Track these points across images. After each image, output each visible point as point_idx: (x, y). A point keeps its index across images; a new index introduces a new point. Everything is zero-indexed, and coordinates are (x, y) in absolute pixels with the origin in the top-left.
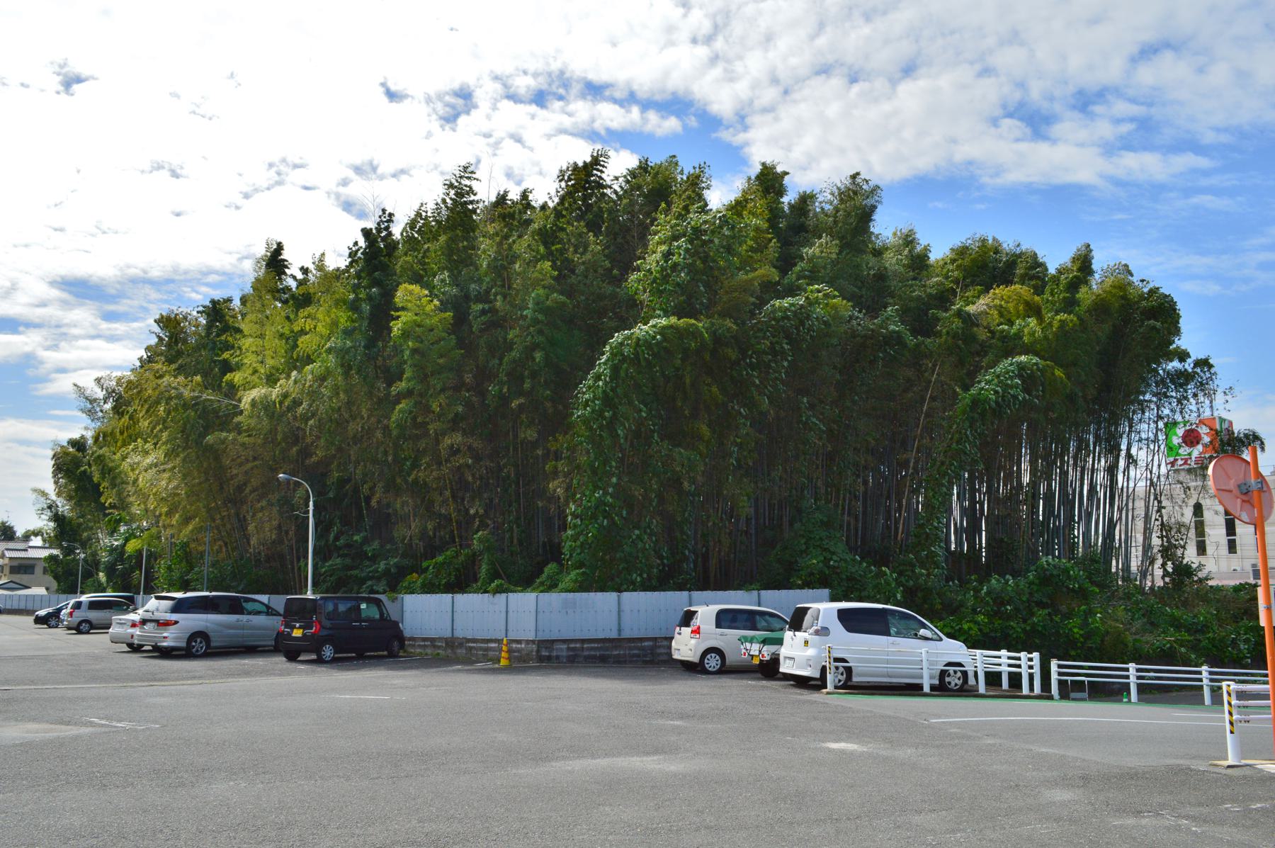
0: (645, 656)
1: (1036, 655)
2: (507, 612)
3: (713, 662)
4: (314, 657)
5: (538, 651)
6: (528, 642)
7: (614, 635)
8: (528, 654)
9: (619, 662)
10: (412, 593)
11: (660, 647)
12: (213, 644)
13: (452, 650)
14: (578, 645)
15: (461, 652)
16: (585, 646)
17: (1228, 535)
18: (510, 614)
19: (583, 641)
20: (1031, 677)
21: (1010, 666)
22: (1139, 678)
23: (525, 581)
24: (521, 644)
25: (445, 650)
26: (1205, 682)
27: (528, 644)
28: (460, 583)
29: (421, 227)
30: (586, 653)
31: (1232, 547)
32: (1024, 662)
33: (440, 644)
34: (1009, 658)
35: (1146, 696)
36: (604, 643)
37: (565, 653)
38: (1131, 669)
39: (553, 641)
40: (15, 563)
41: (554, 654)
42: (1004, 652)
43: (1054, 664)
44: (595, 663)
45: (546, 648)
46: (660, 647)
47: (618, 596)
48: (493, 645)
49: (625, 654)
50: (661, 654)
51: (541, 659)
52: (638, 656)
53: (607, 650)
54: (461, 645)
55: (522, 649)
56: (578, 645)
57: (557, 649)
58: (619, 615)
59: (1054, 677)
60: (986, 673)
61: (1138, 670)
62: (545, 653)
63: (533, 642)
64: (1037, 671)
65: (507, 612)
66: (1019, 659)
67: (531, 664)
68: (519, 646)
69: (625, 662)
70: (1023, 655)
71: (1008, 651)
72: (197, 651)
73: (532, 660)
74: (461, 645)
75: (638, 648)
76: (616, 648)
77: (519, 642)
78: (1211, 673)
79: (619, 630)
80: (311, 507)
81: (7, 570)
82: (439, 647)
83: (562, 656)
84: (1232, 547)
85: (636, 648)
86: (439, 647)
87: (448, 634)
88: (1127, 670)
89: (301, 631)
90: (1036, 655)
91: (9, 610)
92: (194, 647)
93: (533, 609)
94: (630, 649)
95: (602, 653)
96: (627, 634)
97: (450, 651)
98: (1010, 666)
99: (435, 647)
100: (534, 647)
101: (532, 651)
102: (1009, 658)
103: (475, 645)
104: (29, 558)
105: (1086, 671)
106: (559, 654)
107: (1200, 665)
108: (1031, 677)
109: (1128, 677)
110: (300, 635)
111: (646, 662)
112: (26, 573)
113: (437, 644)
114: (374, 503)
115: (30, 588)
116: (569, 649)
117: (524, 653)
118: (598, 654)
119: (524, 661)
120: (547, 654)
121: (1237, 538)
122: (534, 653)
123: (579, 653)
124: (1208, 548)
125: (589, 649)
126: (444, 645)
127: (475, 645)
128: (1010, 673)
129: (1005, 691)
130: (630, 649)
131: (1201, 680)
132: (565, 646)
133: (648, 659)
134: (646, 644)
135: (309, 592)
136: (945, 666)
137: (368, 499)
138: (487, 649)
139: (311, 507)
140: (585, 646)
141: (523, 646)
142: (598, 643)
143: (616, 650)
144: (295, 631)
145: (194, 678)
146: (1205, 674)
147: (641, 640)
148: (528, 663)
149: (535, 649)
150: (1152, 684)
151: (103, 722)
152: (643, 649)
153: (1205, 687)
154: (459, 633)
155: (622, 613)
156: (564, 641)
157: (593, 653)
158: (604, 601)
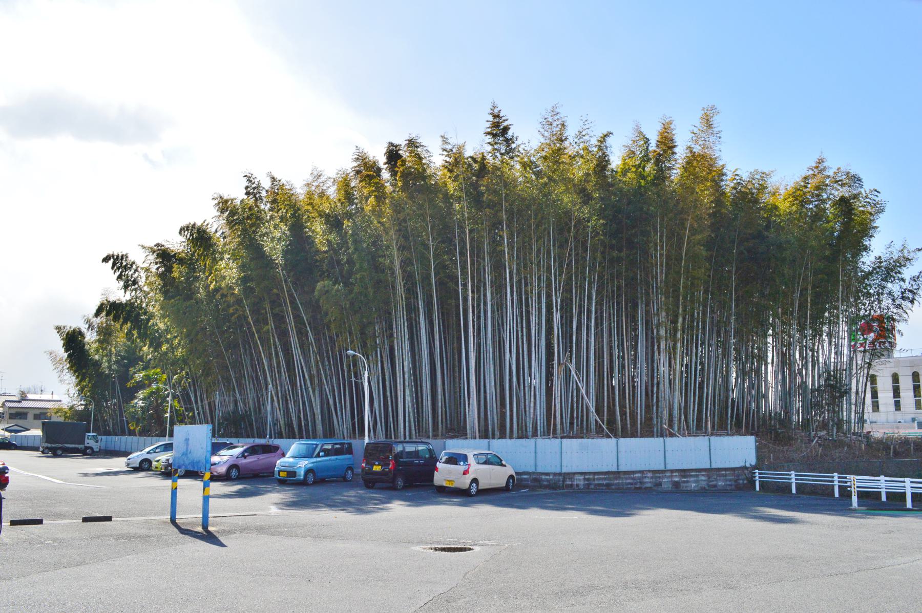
0: (636, 484)
2: (536, 452)
4: (391, 485)
6: (555, 474)
7: (614, 469)
14: (591, 477)
16: (596, 477)
17: (895, 397)
18: (539, 455)
19: (595, 473)
21: (886, 489)
22: (796, 479)
24: (549, 476)
26: (836, 483)
30: (596, 482)
31: (898, 405)
34: (912, 482)
39: (574, 474)
40: (13, 411)
41: (575, 483)
42: (882, 478)
48: (525, 477)
50: (647, 482)
53: (611, 480)
55: (551, 479)
56: (591, 477)
58: (617, 454)
60: (912, 494)
61: (796, 475)
63: (560, 474)
65: (536, 452)
68: (548, 477)
81: (6, 416)
84: (898, 405)
85: (630, 478)
89: (380, 467)
91: (31, 447)
95: (607, 482)
96: (622, 468)
101: (559, 481)
104: (23, 408)
107: (790, 471)
109: (832, 481)
110: (379, 470)
112: (20, 419)
115: (29, 430)
116: (585, 479)
117: (551, 482)
118: (605, 482)
120: (570, 483)
121: (901, 400)
122: (561, 483)
124: (880, 407)
125: (599, 479)
128: (796, 483)
130: (626, 479)
134: (637, 475)
140: (596, 477)
142: (605, 475)
144: (375, 467)
146: (836, 478)
149: (561, 480)
152: (634, 479)
156: (581, 474)
157: (601, 482)
158: (607, 445)
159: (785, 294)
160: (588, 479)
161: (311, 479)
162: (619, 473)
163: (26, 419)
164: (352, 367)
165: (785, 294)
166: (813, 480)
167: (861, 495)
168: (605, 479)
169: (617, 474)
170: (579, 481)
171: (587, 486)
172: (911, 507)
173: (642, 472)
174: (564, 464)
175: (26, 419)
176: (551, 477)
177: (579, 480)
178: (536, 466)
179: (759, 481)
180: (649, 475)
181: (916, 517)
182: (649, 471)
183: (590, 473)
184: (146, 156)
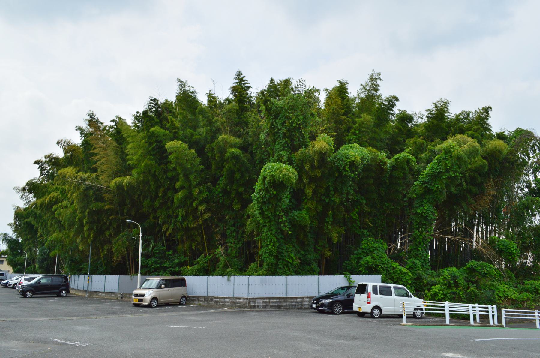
0: (298, 306)
1: (495, 306)
3: (376, 312)
5: (249, 303)
6: (244, 299)
7: (284, 296)
8: (244, 305)
9: (286, 309)
10: (322, 275)
11: (305, 301)
12: (383, 313)
13: (207, 302)
14: (268, 300)
15: (212, 303)
16: (271, 301)
19: (270, 299)
20: (493, 316)
21: (480, 311)
23: (242, 270)
24: (241, 300)
25: (204, 302)
27: (244, 300)
28: (207, 271)
29: (268, 91)
30: (271, 304)
32: (490, 310)
33: (201, 299)
34: (480, 307)
35: (454, 320)
36: (279, 299)
37: (261, 304)
38: (536, 313)
39: (256, 299)
41: (257, 304)
43: (503, 311)
44: (276, 309)
45: (253, 302)
46: (305, 301)
47: (286, 278)
49: (289, 305)
51: (250, 307)
52: (295, 306)
53: (281, 303)
54: (212, 300)
56: (268, 300)
57: (258, 302)
59: (503, 316)
62: (252, 304)
63: (247, 299)
64: (495, 313)
66: (487, 308)
67: (246, 309)
68: (240, 301)
69: (289, 309)
70: (490, 306)
71: (479, 304)
72: (153, 305)
73: (246, 307)
74: (212, 300)
75: (296, 302)
76: (285, 302)
77: (240, 299)
78: (506, 311)
79: (286, 293)
80: (141, 235)
82: (201, 301)
83: (260, 306)
86: (201, 301)
87: (205, 295)
88: (534, 313)
90: (495, 306)
92: (152, 304)
93: (247, 283)
94: (292, 302)
95: (278, 304)
97: (206, 303)
98: (480, 311)
99: (199, 300)
100: (247, 301)
101: (246, 303)
102: (480, 307)
103: (218, 300)
105: (519, 314)
106: (259, 304)
108: (493, 316)
111: (298, 308)
113: (200, 299)
114: (168, 234)
116: (263, 302)
119: (243, 308)
120: (254, 304)
122: (247, 304)
123: (268, 304)
126: (203, 300)
127: (218, 300)
128: (480, 315)
129: (478, 323)
130: (292, 302)
131: (535, 316)
132: (261, 301)
133: (300, 307)
134: (299, 300)
135: (55, 274)
136: (414, 310)
137: (165, 232)
138: (225, 302)
139: (141, 235)
140: (271, 301)
141: (242, 301)
142: (277, 300)
143: (285, 303)
145: (91, 315)
146: (537, 314)
147: (297, 298)
148: (245, 309)
149: (248, 302)
150: (523, 319)
151: (62, 342)
153: (537, 320)
154: (211, 294)
155: (287, 286)
157: (274, 304)
159: (274, 127)
160: (266, 302)
161: (154, 303)
162: (286, 298)
163: (3, 264)
164: (438, 266)
165: (274, 127)
166: (523, 316)
167: (452, 316)
168: (276, 302)
169: (285, 299)
170: (260, 303)
171: (264, 307)
172: (539, 328)
173: (303, 298)
174: (250, 292)
175: (3, 264)
176: (242, 301)
177: (260, 302)
178: (234, 293)
179: (506, 318)
180: (308, 300)
181: (185, 310)
182: (308, 297)
183: (267, 298)
184: (193, 87)
